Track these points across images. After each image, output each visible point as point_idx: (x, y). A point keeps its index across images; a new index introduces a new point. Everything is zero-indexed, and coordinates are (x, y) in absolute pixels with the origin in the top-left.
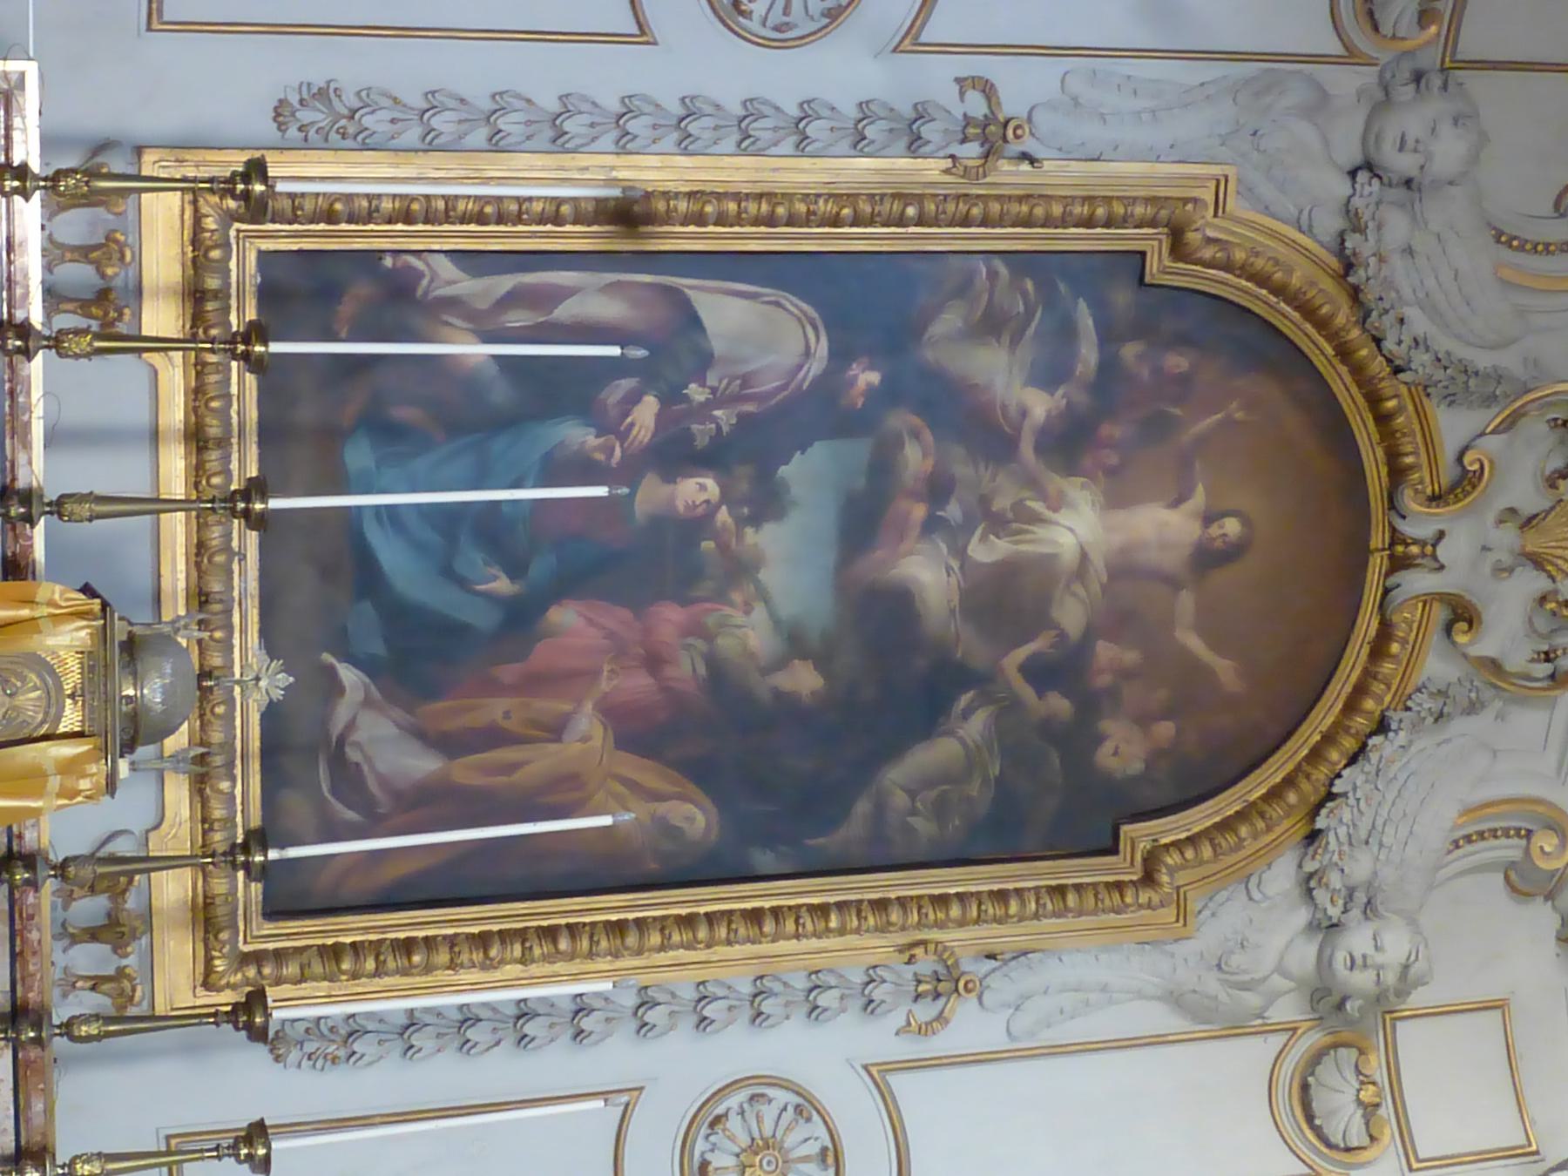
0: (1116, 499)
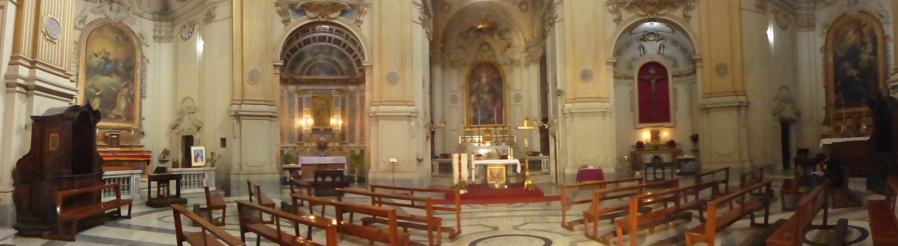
0: (482, 78)
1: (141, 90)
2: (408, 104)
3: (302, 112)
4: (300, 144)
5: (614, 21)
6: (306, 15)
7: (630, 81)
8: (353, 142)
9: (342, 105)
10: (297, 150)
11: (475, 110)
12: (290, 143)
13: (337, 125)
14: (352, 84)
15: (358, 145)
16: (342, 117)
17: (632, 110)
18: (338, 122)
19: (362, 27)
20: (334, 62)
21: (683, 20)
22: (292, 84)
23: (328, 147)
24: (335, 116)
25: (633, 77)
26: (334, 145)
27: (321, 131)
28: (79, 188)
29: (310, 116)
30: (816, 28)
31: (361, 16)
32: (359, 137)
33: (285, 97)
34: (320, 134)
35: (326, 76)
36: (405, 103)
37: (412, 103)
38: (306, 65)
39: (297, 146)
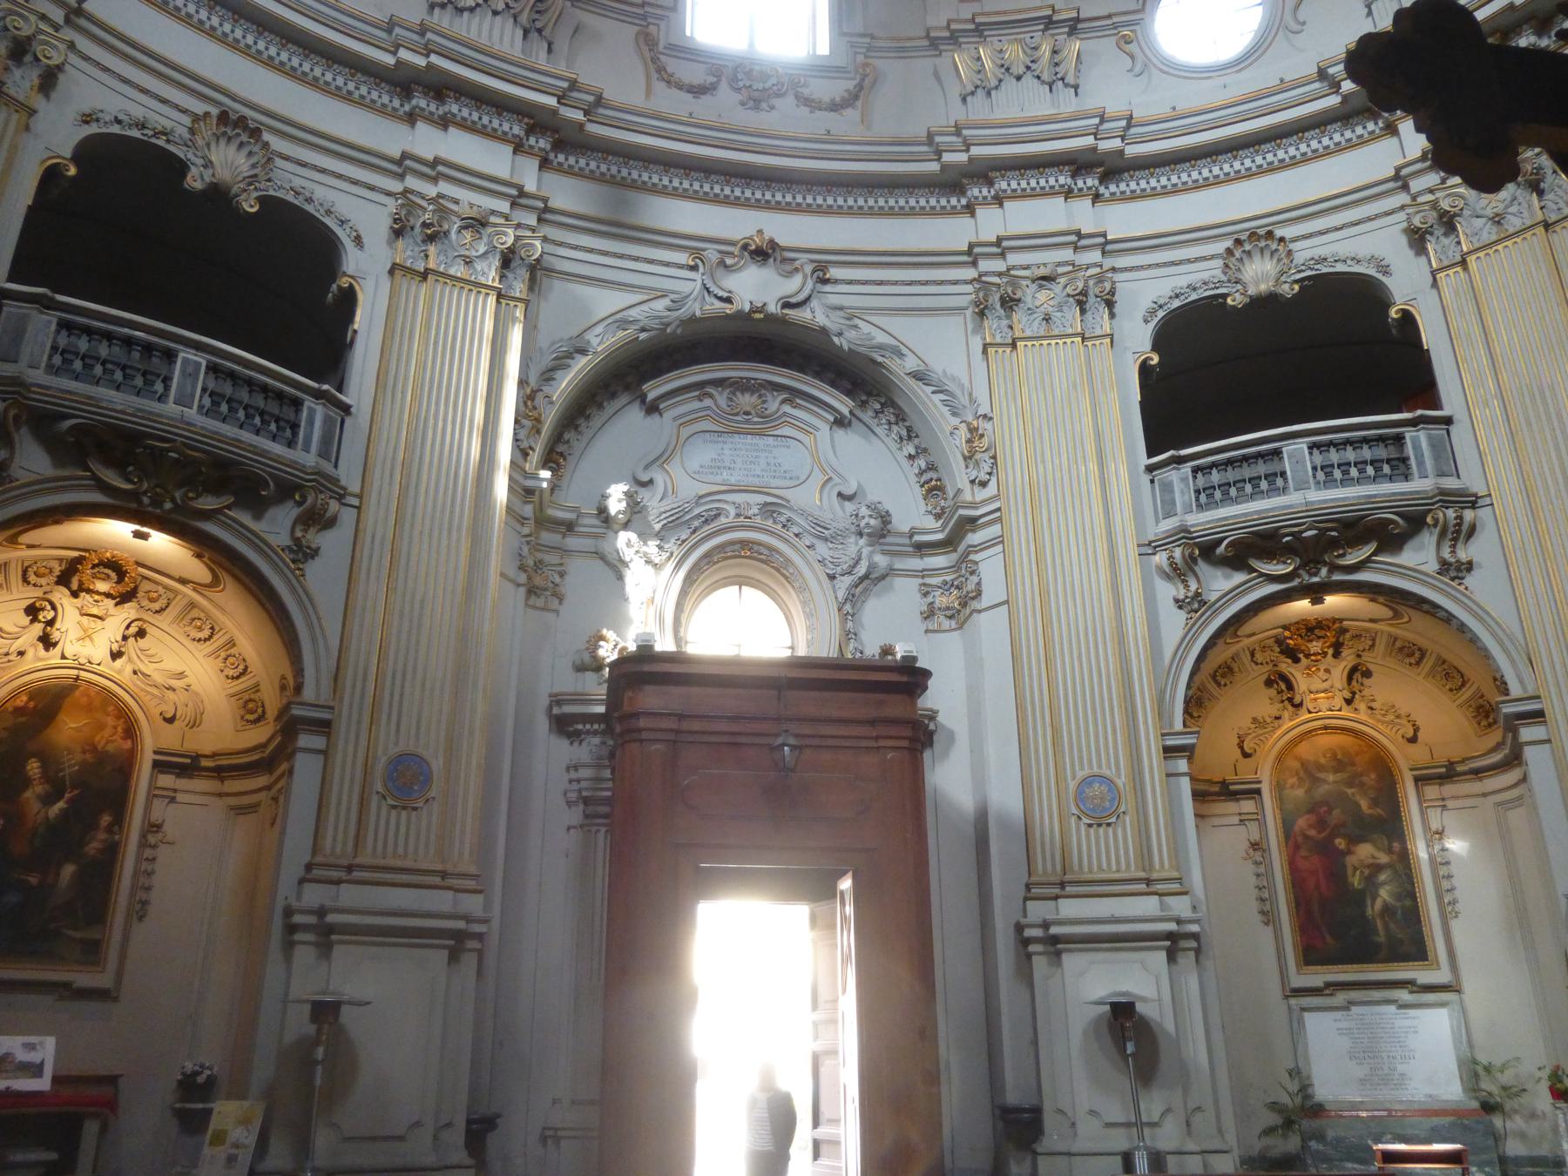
2: (1160, 887)
5: (1180, 604)
6: (87, 469)
7: (1248, 806)
17: (1268, 917)
19: (313, 569)
25: (1258, 792)
31: (1460, 545)
36: (1149, 885)
37: (1175, 887)
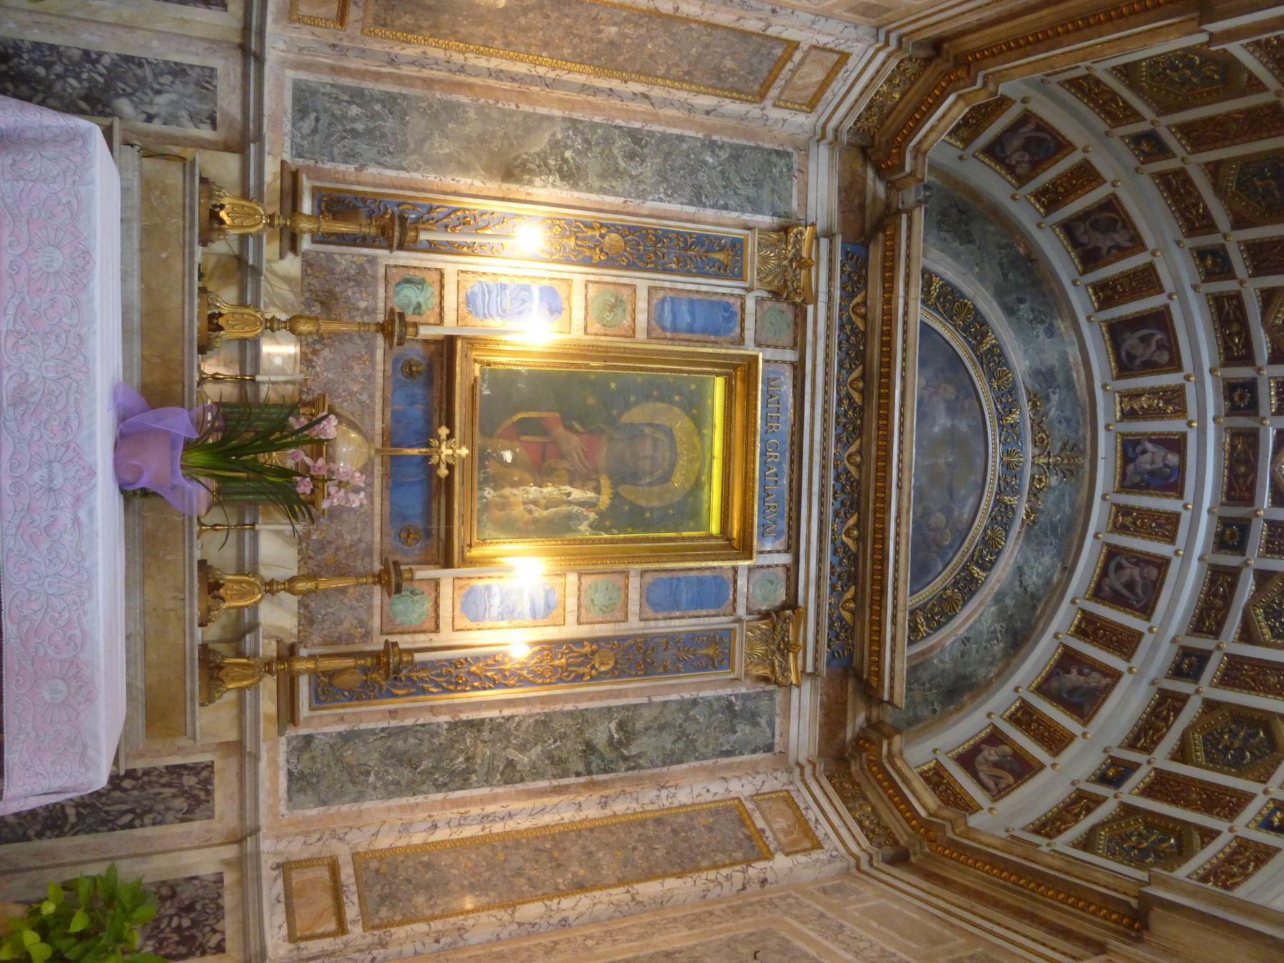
1: (681, 220)
3: (610, 262)
4: (291, 194)
8: (300, 783)
9: (671, 639)
10: (225, 167)
11: (76, 521)
12: (304, 101)
13: (474, 611)
14: (832, 718)
15: (269, 848)
16: (552, 646)
18: (509, 614)
20: (990, 550)
21: (97, 870)
22: (851, 194)
23: (245, 530)
24: (572, 578)
26: (271, 587)
27: (426, 437)
28: (320, 645)
29: (577, 334)
30: (93, 48)
32: (360, 840)
33: (754, 110)
34: (392, 438)
35: (909, 485)
38: (975, 328)
39: (271, 169)
